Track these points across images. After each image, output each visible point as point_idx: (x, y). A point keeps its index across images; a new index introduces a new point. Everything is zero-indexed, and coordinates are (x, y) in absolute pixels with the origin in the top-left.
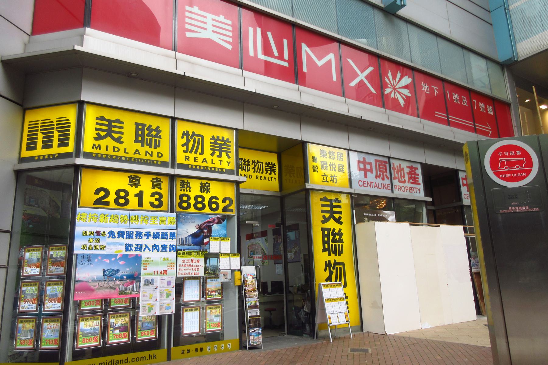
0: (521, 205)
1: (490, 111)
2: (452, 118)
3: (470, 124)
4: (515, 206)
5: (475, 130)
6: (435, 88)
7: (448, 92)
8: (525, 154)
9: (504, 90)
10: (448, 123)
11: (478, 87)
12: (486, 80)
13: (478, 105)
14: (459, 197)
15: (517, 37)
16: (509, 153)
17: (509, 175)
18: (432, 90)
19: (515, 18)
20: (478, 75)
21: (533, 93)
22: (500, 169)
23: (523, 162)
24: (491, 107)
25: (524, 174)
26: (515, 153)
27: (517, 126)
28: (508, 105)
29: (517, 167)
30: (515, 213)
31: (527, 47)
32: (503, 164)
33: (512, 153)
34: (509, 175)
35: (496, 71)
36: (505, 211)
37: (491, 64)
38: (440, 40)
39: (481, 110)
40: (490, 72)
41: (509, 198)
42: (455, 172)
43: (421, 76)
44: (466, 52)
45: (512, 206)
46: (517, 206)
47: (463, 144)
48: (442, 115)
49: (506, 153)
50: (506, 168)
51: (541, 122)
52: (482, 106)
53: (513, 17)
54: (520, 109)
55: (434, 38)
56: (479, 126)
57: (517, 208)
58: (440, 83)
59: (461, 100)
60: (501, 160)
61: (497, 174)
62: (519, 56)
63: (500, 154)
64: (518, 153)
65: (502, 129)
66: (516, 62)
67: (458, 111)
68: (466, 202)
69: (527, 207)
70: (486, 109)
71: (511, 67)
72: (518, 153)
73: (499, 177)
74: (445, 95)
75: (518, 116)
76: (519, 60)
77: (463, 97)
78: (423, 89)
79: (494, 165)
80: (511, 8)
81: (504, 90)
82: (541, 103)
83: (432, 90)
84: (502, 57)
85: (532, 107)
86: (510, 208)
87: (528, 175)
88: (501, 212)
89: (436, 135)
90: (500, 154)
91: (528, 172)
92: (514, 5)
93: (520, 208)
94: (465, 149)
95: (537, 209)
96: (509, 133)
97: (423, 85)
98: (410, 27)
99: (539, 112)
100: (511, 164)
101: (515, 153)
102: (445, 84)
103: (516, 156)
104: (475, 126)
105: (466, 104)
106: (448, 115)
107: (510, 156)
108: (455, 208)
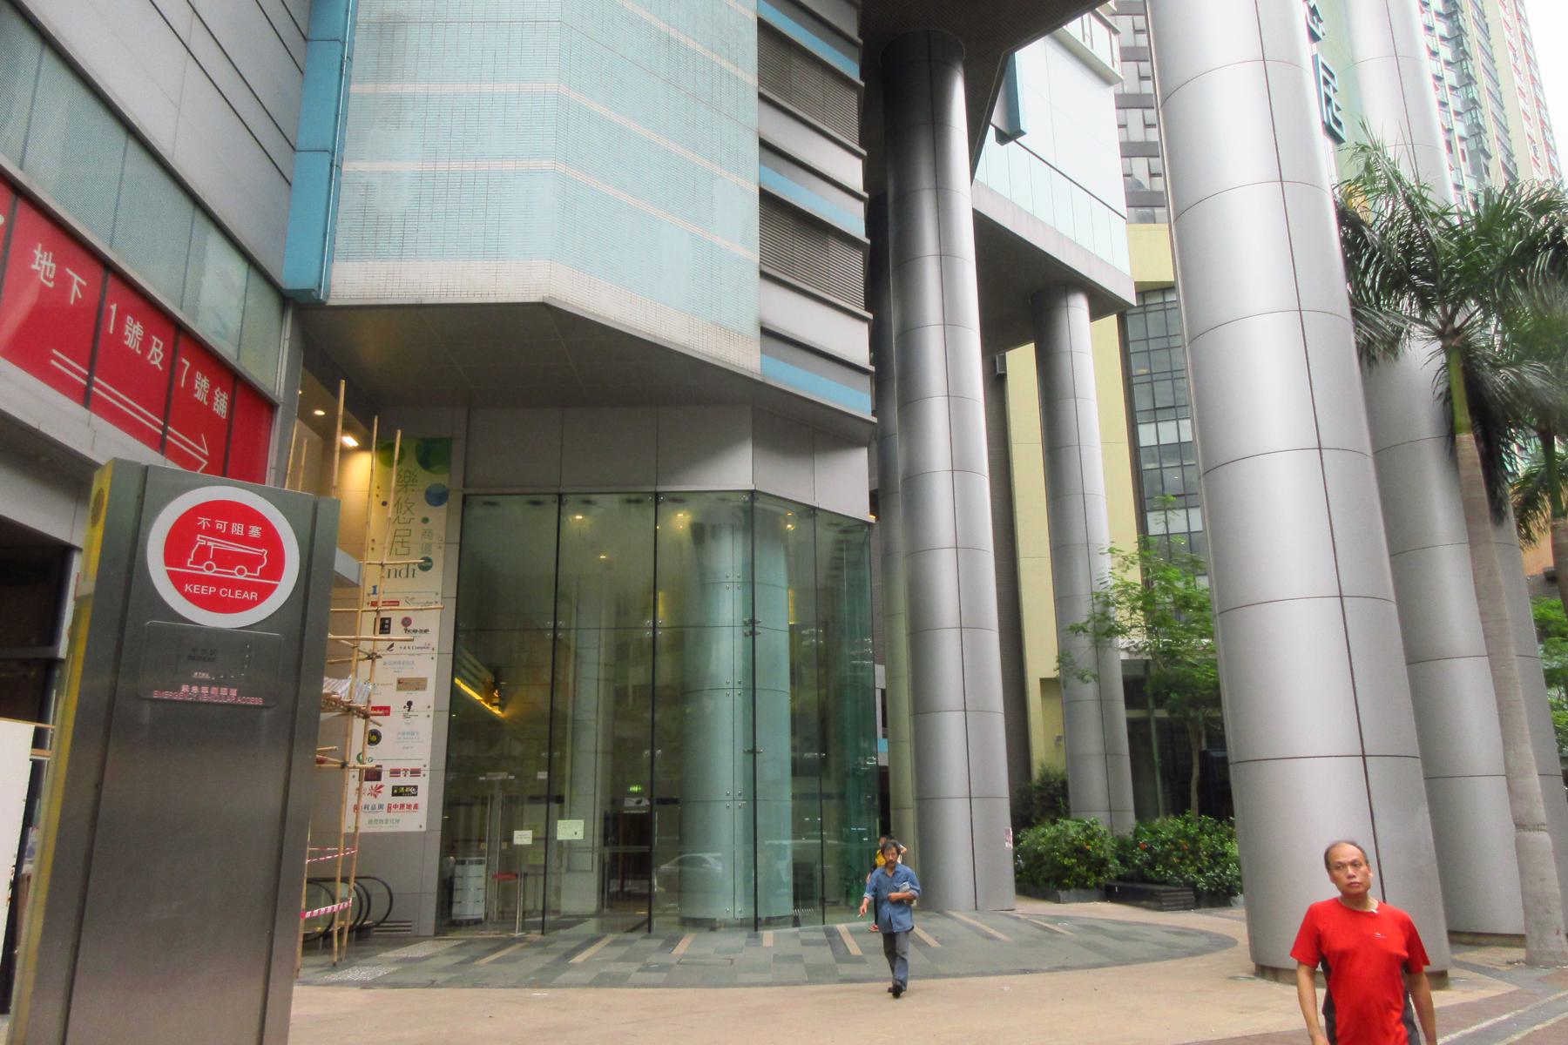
0: (219, 683)
1: (221, 406)
2: (103, 388)
3: (152, 422)
4: (200, 683)
5: (160, 444)
6: (77, 278)
7: (114, 307)
8: (271, 539)
9: (272, 365)
10: (85, 397)
11: (205, 327)
12: (233, 320)
13: (191, 378)
14: (51, 637)
15: (340, 244)
16: (229, 528)
17: (212, 590)
18: (62, 280)
19: (349, 197)
20: (218, 301)
21: (337, 396)
22: (190, 568)
23: (259, 559)
24: (225, 396)
25: (254, 595)
26: (246, 530)
27: (277, 469)
28: (270, 406)
29: (241, 572)
30: (196, 703)
31: (356, 280)
32: (203, 554)
33: (238, 529)
34: (212, 590)
35: (266, 305)
36: (167, 695)
37: (258, 284)
38: (134, 150)
39: (197, 395)
40: (250, 302)
41: (191, 658)
42: (64, 552)
43: (44, 226)
44: (200, 219)
45: (192, 683)
46: (210, 684)
47: (94, 466)
48: (76, 371)
49: (221, 525)
50: (209, 568)
51: (335, 477)
52: (202, 384)
53: (346, 194)
54: (297, 427)
55: (118, 135)
56: (176, 437)
57: (205, 690)
58: (98, 272)
59: (146, 344)
60: (201, 540)
61: (178, 581)
62: (332, 295)
63: (204, 522)
64: (255, 531)
65: (238, 453)
66: (321, 306)
67: (127, 371)
68: (62, 651)
69: (234, 692)
70: (210, 397)
71: (302, 309)
72: (255, 531)
73: (180, 588)
74: (100, 312)
75: (286, 441)
76: (331, 302)
77: (155, 339)
78: (35, 267)
79: (176, 549)
80: (346, 167)
81: (272, 365)
82: (348, 428)
83: (62, 280)
84: (291, 278)
85: (326, 434)
86: (185, 688)
87: (262, 598)
88: (156, 695)
89: (33, 423)
90: (204, 522)
91: (265, 592)
92: (354, 164)
93: (214, 690)
94: (102, 484)
95: (259, 701)
96: (248, 469)
97: (38, 253)
98: (50, 63)
99: (338, 448)
100: (224, 559)
101: (246, 530)
102: (111, 281)
103: (245, 540)
104: (163, 428)
105: (157, 362)
106: (92, 373)
107: (228, 536)
108: (26, 663)
